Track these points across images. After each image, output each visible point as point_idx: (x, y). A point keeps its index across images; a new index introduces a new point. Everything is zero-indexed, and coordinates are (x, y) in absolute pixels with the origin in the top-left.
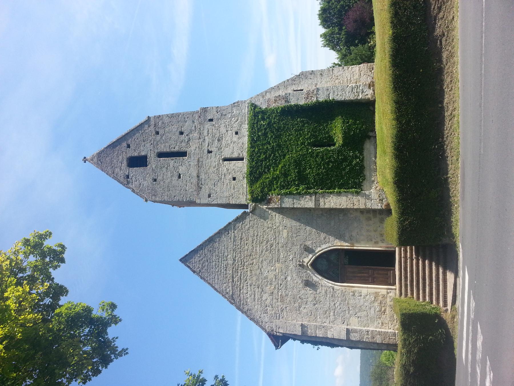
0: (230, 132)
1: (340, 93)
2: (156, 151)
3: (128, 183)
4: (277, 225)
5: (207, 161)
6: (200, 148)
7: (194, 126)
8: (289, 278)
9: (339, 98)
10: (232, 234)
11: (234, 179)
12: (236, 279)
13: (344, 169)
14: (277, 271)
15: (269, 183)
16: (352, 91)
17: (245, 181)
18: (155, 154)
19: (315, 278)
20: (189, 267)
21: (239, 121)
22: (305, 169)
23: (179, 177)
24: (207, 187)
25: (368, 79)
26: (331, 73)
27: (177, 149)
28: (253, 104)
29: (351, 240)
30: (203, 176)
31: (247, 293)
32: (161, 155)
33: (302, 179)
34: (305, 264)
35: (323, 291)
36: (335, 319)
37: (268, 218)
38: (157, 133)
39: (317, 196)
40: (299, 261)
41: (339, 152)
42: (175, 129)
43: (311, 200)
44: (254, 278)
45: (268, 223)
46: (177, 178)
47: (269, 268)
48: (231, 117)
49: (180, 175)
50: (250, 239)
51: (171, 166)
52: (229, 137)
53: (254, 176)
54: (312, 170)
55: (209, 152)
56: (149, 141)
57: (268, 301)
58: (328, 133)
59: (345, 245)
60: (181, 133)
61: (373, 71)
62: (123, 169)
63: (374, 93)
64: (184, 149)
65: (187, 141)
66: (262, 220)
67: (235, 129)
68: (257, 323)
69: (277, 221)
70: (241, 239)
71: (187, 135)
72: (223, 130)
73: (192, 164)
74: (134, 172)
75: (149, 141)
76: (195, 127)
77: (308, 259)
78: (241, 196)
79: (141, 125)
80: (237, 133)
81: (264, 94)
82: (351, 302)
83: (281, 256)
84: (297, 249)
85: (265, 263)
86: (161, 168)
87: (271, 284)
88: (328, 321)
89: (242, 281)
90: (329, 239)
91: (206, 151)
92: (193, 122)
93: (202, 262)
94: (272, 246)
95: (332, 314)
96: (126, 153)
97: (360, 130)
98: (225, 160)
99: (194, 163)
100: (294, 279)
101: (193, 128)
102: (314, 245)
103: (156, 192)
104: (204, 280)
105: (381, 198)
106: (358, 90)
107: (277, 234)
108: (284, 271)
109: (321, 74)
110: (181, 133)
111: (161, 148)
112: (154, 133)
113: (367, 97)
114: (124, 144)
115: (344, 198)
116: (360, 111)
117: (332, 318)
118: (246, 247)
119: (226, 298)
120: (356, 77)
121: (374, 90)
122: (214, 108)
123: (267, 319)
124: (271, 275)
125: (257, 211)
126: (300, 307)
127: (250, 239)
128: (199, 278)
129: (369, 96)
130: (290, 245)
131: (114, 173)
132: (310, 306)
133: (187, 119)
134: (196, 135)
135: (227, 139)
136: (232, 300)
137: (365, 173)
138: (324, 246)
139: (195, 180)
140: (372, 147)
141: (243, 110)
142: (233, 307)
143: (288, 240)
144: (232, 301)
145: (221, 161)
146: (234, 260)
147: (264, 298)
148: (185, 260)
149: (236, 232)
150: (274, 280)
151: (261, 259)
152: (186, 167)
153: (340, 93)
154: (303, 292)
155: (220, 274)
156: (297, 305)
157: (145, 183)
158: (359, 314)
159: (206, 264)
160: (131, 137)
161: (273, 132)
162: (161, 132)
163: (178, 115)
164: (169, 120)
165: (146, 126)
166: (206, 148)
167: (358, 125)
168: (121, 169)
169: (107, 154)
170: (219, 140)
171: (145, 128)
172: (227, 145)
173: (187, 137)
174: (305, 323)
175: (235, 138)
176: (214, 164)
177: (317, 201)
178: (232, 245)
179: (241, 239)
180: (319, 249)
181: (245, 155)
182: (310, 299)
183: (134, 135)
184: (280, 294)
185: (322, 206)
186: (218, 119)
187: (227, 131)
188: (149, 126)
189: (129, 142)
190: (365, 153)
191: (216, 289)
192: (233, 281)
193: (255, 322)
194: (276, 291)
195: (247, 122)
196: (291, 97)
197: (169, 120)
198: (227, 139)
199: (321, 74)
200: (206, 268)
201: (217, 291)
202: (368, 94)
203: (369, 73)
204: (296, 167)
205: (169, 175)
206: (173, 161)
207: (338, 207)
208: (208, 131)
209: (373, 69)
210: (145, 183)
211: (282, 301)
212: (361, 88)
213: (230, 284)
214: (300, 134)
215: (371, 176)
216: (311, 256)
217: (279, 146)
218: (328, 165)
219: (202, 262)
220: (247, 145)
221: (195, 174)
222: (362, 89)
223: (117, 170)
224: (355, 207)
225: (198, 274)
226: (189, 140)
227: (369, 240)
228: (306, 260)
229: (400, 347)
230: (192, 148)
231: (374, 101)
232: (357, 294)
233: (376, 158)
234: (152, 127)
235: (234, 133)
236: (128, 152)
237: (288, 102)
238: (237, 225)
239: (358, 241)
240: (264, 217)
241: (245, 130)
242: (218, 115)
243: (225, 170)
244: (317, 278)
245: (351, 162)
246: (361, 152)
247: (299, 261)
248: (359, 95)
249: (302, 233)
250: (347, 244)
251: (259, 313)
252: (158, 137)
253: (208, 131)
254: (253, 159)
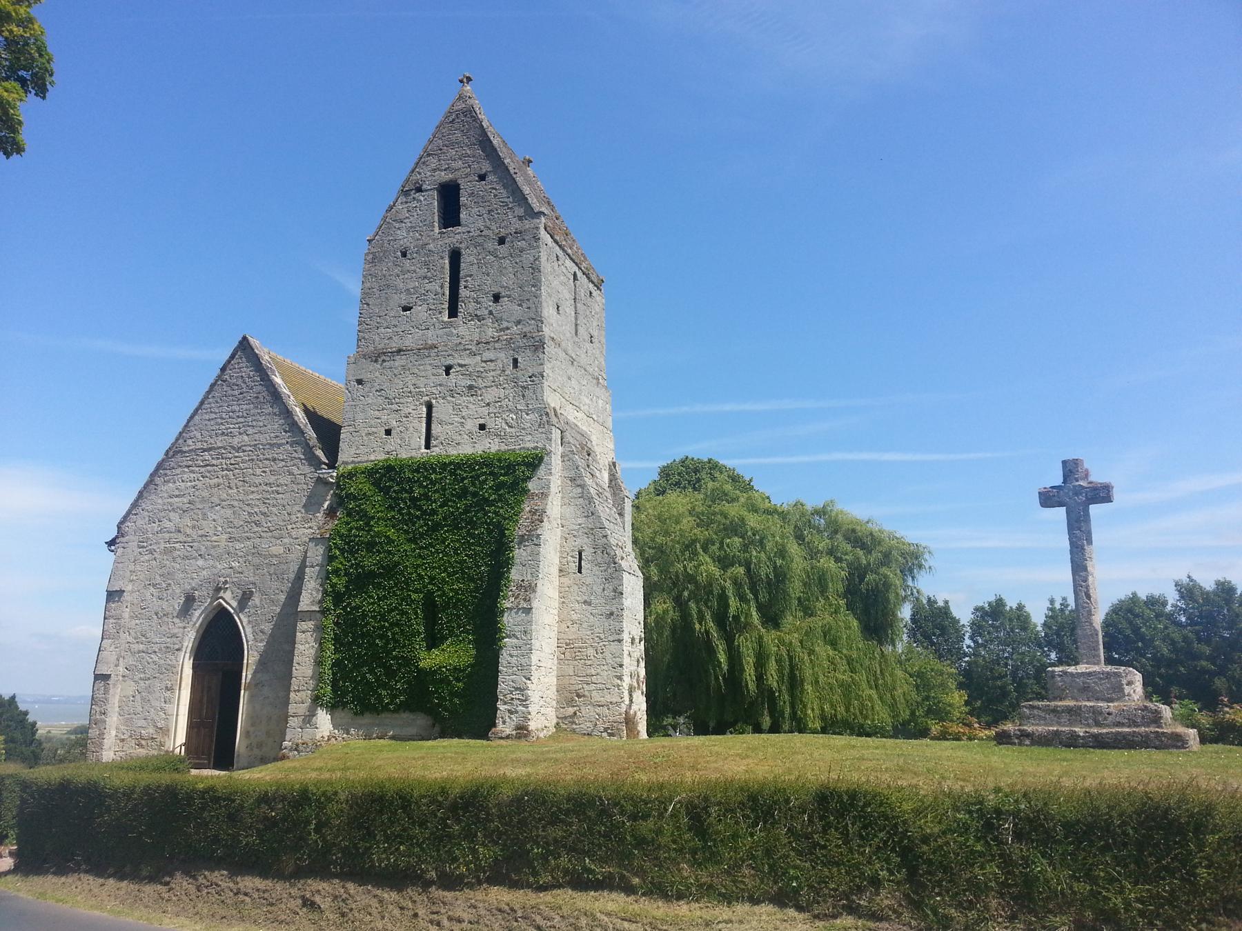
0: (485, 410)
1: (514, 660)
2: (462, 246)
3: (406, 193)
4: (294, 533)
5: (429, 368)
6: (459, 348)
7: (509, 325)
8: (200, 562)
9: (504, 658)
10: (285, 437)
11: (388, 432)
12: (207, 456)
13: (371, 671)
14: (215, 538)
15: (362, 510)
16: (517, 689)
17: (383, 457)
18: (457, 245)
19: (197, 613)
20: (233, 357)
21: (508, 430)
22: (378, 586)
23: (406, 309)
24: (377, 374)
25: (589, 724)
26: (611, 638)
27: (463, 292)
28: (541, 459)
29: (255, 685)
30: (400, 361)
31: (183, 481)
32: (455, 257)
33: (361, 581)
34: (221, 594)
35: (176, 631)
36: (133, 654)
37: (307, 512)
38: (502, 241)
39: (318, 615)
40: (226, 582)
41: (408, 662)
42: (508, 280)
43: (312, 603)
44: (205, 494)
45: (298, 513)
46: (404, 303)
47: (220, 521)
48: (517, 412)
49: (409, 309)
50: (272, 479)
51: (428, 287)
52: (475, 411)
53: (387, 476)
54: (373, 604)
55: (448, 370)
56: (488, 223)
57: (167, 524)
58: (451, 634)
59: (247, 675)
60: (497, 298)
61: (605, 734)
62: (434, 177)
63: (501, 738)
64: (462, 308)
65: (479, 313)
66: (304, 500)
67: (490, 424)
68: (135, 505)
69: (302, 531)
70: (274, 460)
71: (491, 313)
72: (490, 395)
73: (430, 333)
74: (431, 203)
75: (488, 223)
76: (508, 328)
77: (229, 600)
78: (353, 451)
79: (522, 199)
80: (482, 427)
81: (578, 482)
82: (157, 684)
83: (238, 545)
84: (250, 576)
85: (229, 512)
86: (426, 264)
87: (194, 527)
88: (130, 639)
89: (203, 470)
90: (261, 641)
91: (449, 362)
92: (518, 322)
93: (240, 382)
94: (257, 524)
95: (141, 647)
96: (467, 175)
97: (439, 705)
98: (430, 407)
99: (431, 336)
100: (196, 573)
101: (505, 324)
102: (252, 611)
103: (381, 261)
104: (209, 392)
105: (301, 748)
106: (516, 702)
107: (276, 533)
108: (212, 552)
109: (612, 614)
110: (497, 298)
111: (470, 255)
112: (503, 232)
113: (499, 721)
114: (486, 167)
115: (310, 672)
116: (471, 704)
117: (136, 647)
118: (258, 471)
119: (177, 440)
120: (596, 697)
121: (508, 737)
122: (540, 369)
123: (140, 522)
124: (208, 526)
125: (321, 488)
126: (154, 586)
127: (272, 479)
128: (212, 381)
129: (500, 726)
130: (256, 561)
131: (429, 155)
132: (156, 604)
133: (525, 305)
134: (491, 332)
135: (471, 406)
136: (173, 452)
137: (367, 715)
138: (249, 630)
139: (395, 344)
140: (413, 731)
141: (530, 437)
142: (161, 456)
143: (265, 557)
144: (171, 453)
145: (426, 398)
146: (238, 449)
147: (172, 514)
148: (244, 345)
149: (288, 447)
150: (200, 532)
151: (236, 503)
152: (428, 319)
153: (514, 660)
154: (178, 591)
155: (217, 424)
156: (158, 580)
157: (401, 234)
158: (138, 697)
159: (236, 393)
160: (501, 179)
161: (466, 511)
162: (503, 250)
163: (537, 285)
164: (527, 264)
165: (521, 212)
166: (456, 361)
167: (451, 701)
168: (434, 170)
169: (468, 130)
170: (470, 387)
171: (516, 209)
172: (457, 408)
173: (486, 312)
174: (126, 596)
175: (471, 425)
176: (421, 382)
177: (309, 615)
178: (265, 442)
179: (274, 460)
180: (245, 620)
181: (436, 451)
182: (165, 605)
183: (505, 187)
184: (177, 545)
185: (302, 626)
186: (515, 381)
187: (488, 404)
188: (520, 218)
189: (491, 178)
190: (405, 716)
191: (192, 417)
192: (204, 450)
193: (136, 501)
194: (182, 538)
195: (504, 447)
196: (529, 549)
197: (527, 264)
198: (471, 406)
199: (612, 614)
200: (230, 392)
201: (189, 421)
202: (505, 726)
203: (601, 727)
204: (383, 568)
205: (411, 285)
206: (439, 290)
207: (296, 659)
208: (491, 361)
209: (611, 735)
210: (401, 234)
211: (167, 551)
212: (521, 708)
213: (199, 445)
214: (455, 573)
215: (359, 727)
216: (235, 604)
217: (436, 527)
218: (381, 637)
219: (240, 382)
220: (455, 452)
221: (409, 342)
222: (517, 712)
223: (433, 162)
224: (292, 695)
225: (219, 377)
226: (480, 318)
227: (253, 719)
228: (228, 595)
229: (211, 775)
230: (464, 329)
231: (488, 739)
232: (168, 694)
233: (393, 738)
234: (517, 225)
235: (482, 421)
236: (470, 178)
237: (520, 543)
238: (299, 449)
239: (252, 699)
240: (311, 505)
241: (489, 446)
242: (524, 379)
243: (407, 410)
244: (198, 616)
245: (385, 686)
246: (405, 707)
247: (226, 582)
248: (505, 703)
249: (275, 585)
250: (249, 677)
251: (150, 508)
252: (491, 245)
253: (491, 361)
254: (418, 472)
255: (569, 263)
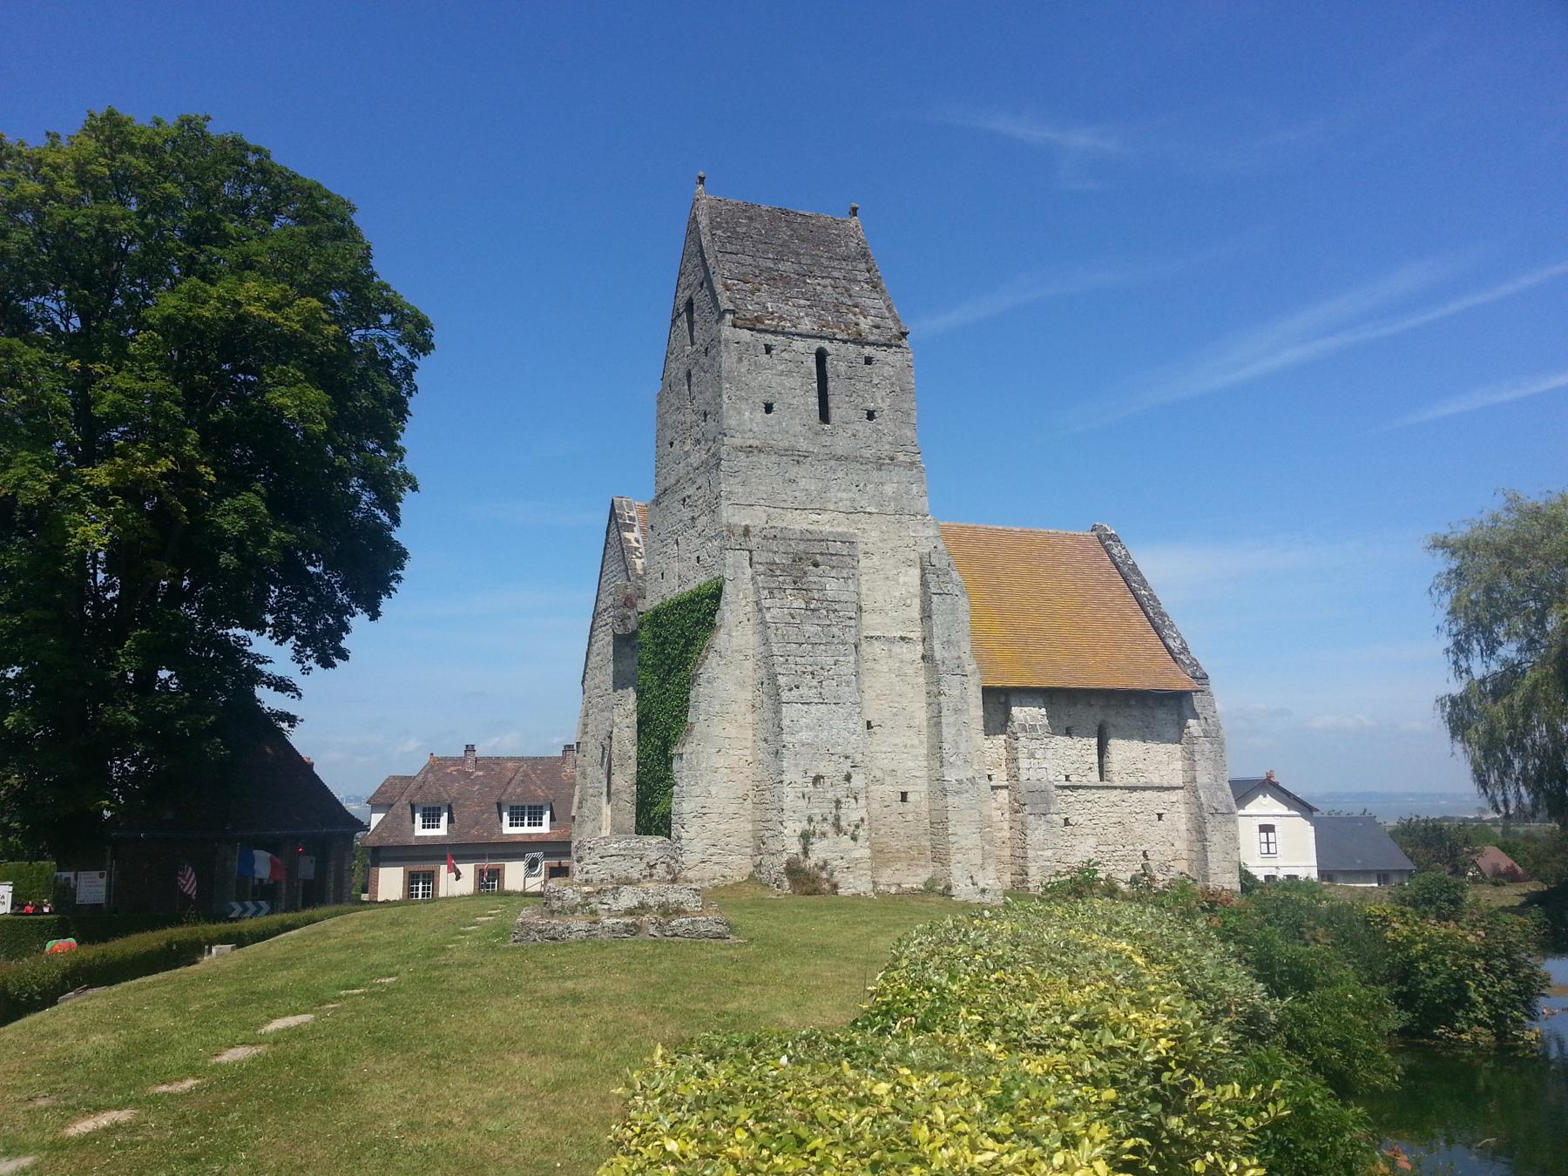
28: (720, 589)
255: (799, 344)
